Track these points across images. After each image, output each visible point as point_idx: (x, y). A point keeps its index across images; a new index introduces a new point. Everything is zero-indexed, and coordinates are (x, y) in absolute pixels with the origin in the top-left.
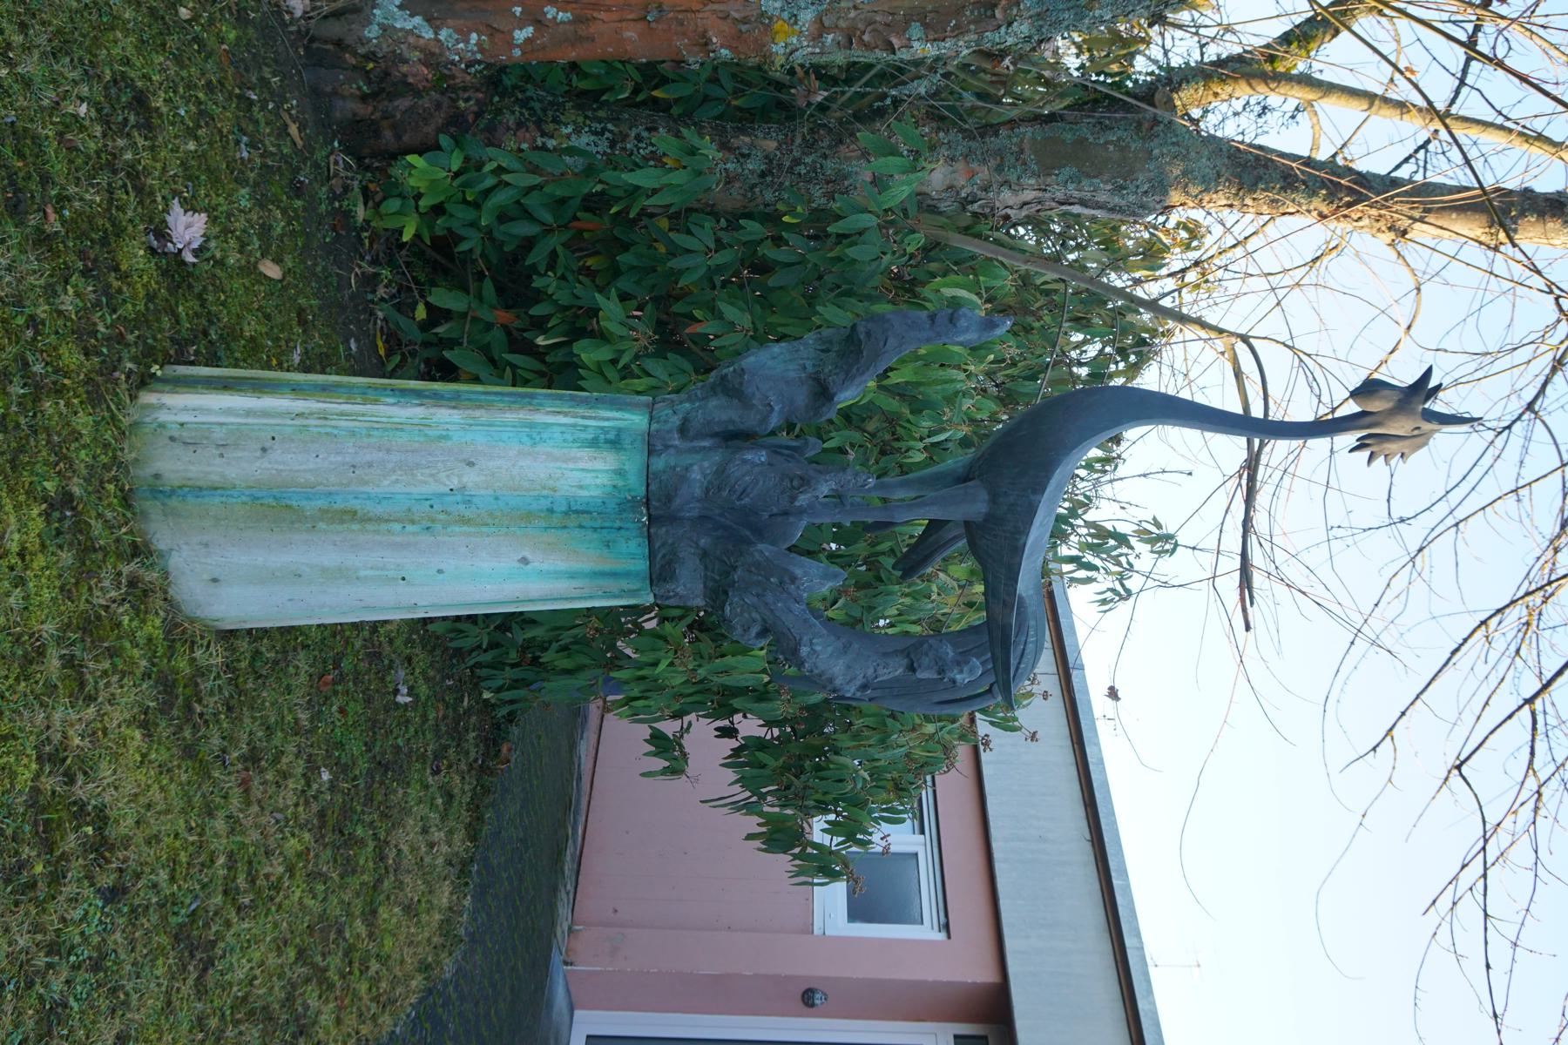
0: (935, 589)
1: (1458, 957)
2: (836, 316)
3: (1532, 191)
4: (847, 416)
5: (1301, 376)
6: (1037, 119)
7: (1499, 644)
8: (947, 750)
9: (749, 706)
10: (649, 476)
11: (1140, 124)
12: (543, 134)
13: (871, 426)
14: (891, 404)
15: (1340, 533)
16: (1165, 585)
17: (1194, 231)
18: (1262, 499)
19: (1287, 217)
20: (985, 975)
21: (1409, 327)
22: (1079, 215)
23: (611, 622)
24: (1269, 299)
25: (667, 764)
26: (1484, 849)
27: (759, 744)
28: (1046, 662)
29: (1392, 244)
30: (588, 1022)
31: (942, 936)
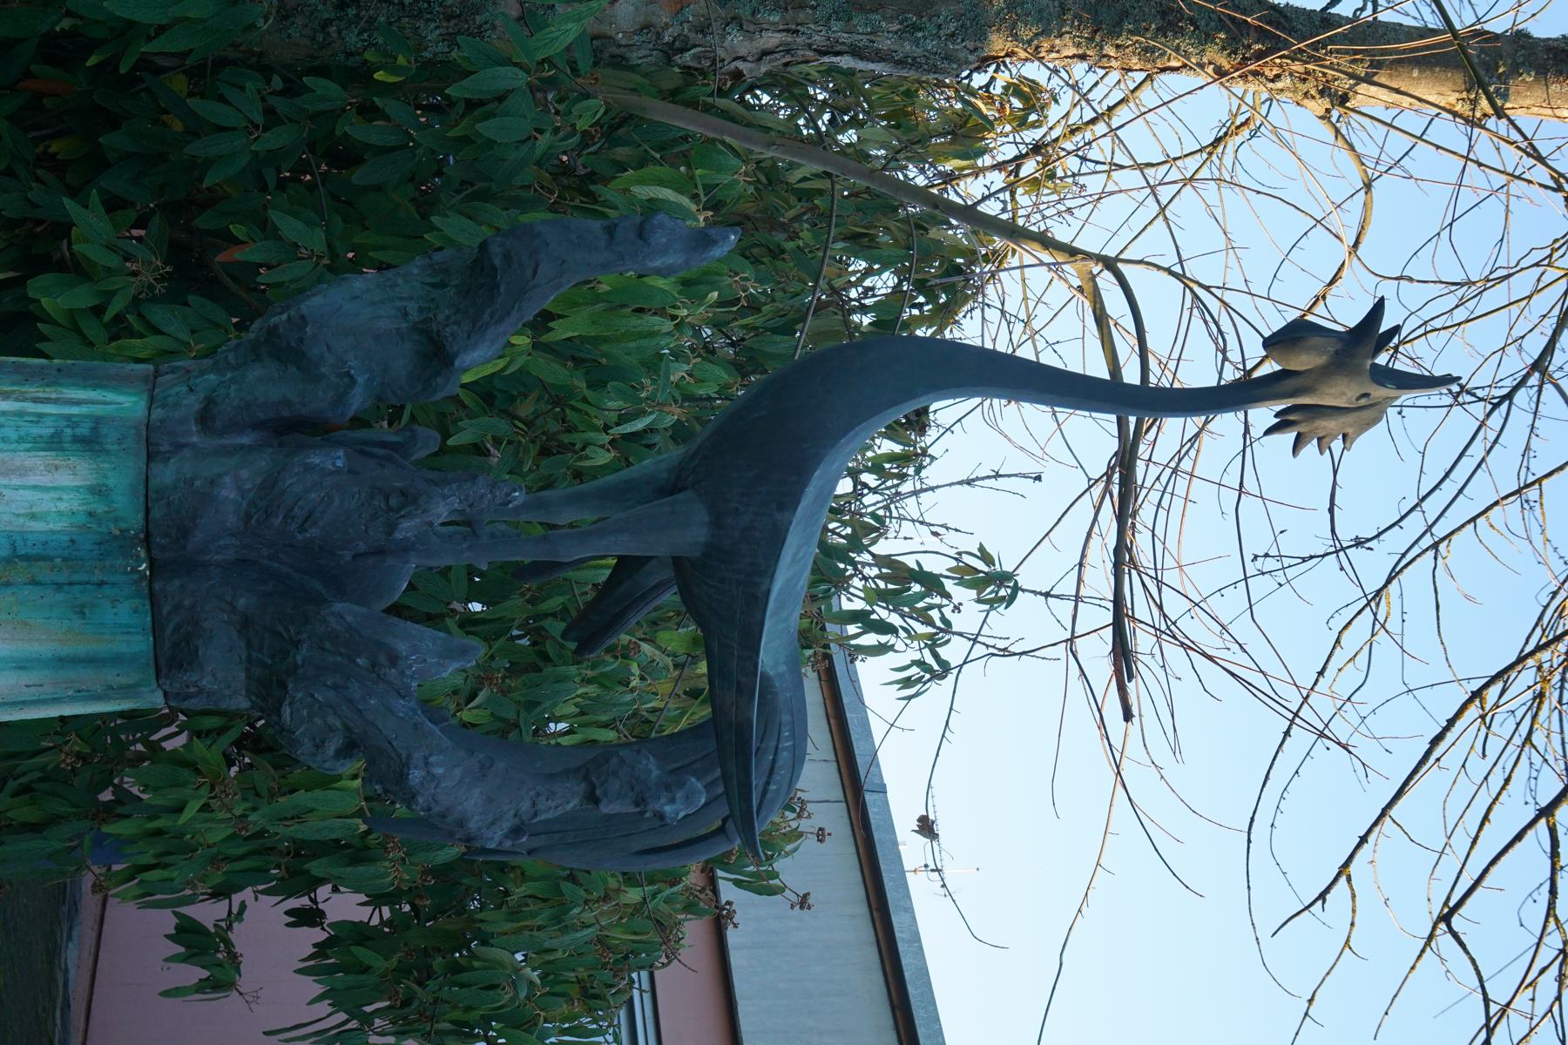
0: (635, 669)
2: (458, 230)
3: (1528, 36)
4: (489, 394)
5: (1197, 322)
7: (1503, 725)
8: (665, 929)
9: (337, 871)
10: (149, 496)
13: (526, 409)
14: (555, 372)
15: (1271, 564)
16: (1006, 653)
17: (1031, 98)
21: (1356, 245)
22: (851, 72)
25: (205, 974)
27: (358, 934)
28: (816, 778)
29: (1326, 117)
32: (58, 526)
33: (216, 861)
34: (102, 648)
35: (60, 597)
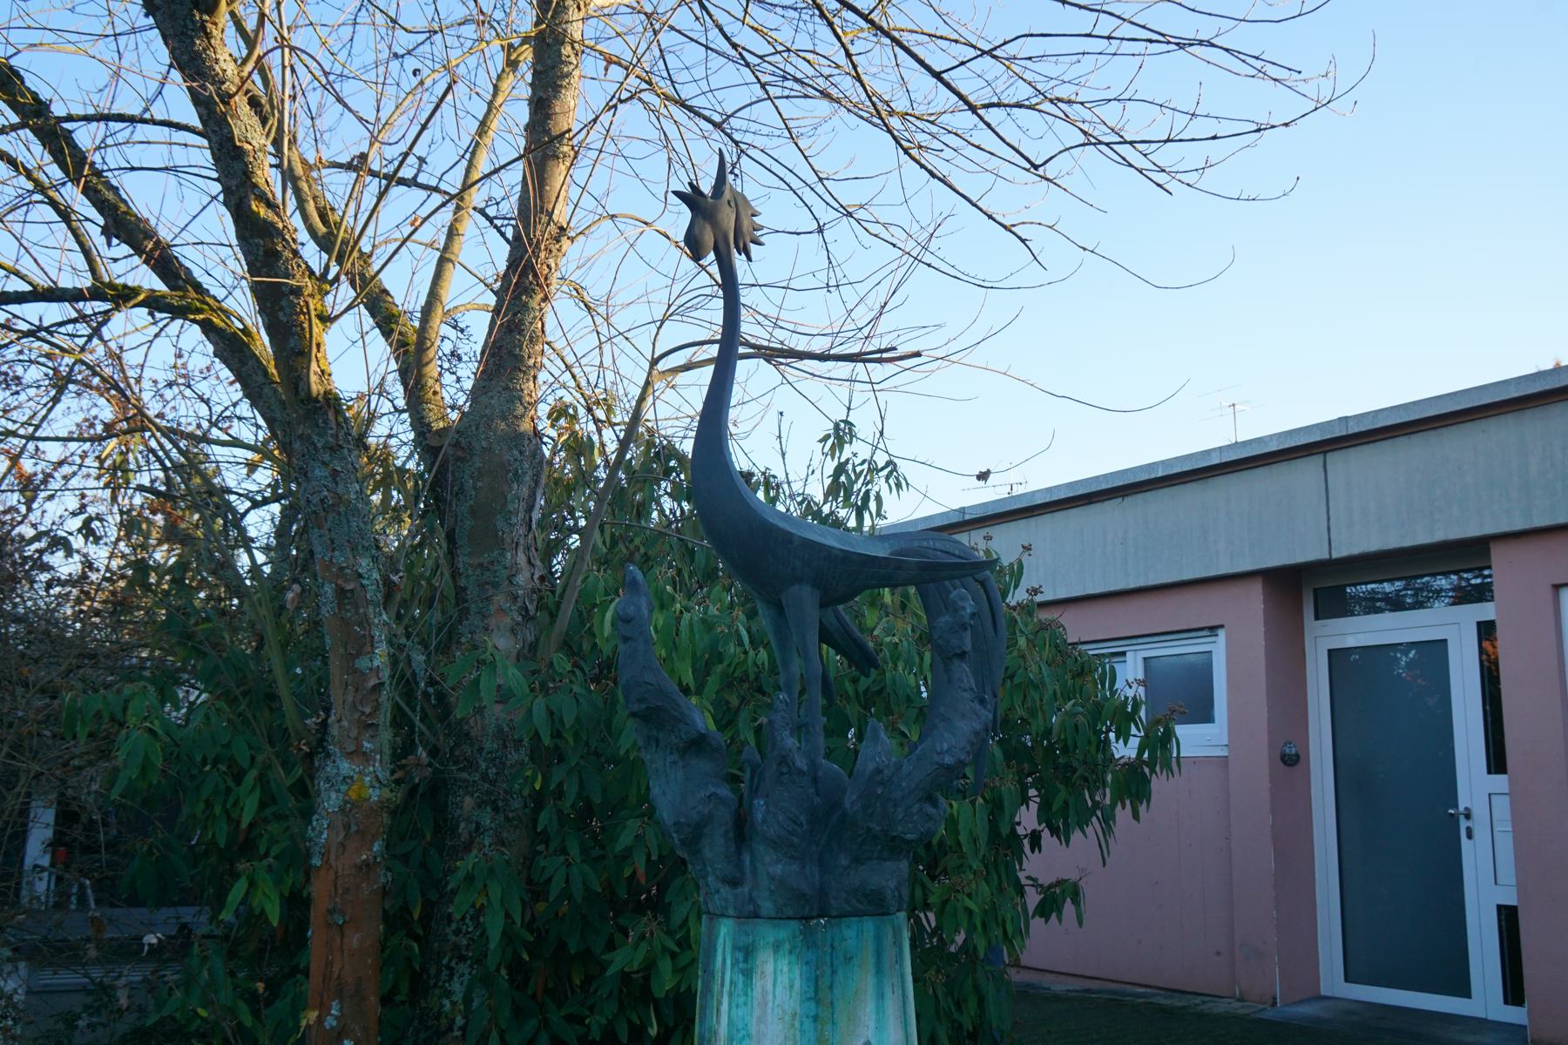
0: (888, 639)
1: (1209, 165)
2: (629, 737)
4: (726, 720)
6: (451, 554)
8: (1044, 626)
9: (1007, 818)
10: (779, 917)
11: (459, 459)
12: (450, 1029)
14: (713, 683)
17: (560, 412)
18: (800, 344)
19: (547, 328)
20: (1255, 594)
23: (929, 957)
24: (619, 338)
26: (1107, 144)
27: (1045, 813)
29: (572, 239)
30: (1332, 980)
31: (1222, 633)
32: (797, 973)
33: (1001, 889)
34: (871, 947)
35: (840, 972)
